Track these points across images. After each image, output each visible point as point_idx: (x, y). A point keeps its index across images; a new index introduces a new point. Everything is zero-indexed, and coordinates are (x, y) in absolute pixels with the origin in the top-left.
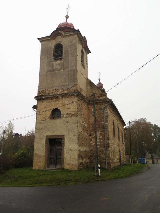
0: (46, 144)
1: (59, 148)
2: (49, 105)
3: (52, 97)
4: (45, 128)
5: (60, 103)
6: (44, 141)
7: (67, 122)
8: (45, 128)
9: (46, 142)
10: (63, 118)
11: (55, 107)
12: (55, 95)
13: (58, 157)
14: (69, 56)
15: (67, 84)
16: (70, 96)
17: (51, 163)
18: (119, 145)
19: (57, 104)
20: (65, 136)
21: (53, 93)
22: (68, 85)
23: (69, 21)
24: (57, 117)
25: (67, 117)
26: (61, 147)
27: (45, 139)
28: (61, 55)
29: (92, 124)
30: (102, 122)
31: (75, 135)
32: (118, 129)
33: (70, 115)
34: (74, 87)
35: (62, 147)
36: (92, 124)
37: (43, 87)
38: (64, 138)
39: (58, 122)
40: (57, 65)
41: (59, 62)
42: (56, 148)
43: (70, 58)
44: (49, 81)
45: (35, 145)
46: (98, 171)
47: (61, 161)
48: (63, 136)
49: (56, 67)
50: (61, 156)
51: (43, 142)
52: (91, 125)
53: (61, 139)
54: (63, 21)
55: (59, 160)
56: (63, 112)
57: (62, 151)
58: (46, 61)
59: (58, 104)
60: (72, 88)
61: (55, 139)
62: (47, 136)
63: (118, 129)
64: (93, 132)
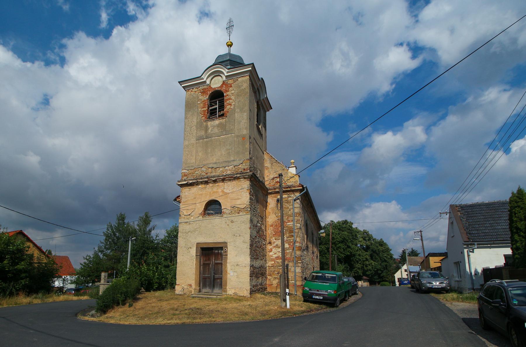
0: (196, 256)
1: (218, 262)
2: (201, 195)
3: (206, 181)
4: (195, 231)
5: (220, 190)
6: (193, 251)
7: (232, 222)
8: (195, 231)
9: (196, 253)
10: (225, 216)
11: (213, 198)
12: (212, 177)
13: (216, 276)
14: (235, 111)
15: (232, 159)
16: (238, 178)
17: (205, 286)
18: (313, 259)
19: (214, 192)
20: (228, 244)
21: (209, 174)
22: (234, 161)
23: (234, 51)
24: (218, 213)
25: (231, 213)
26: (222, 260)
27: (195, 248)
28: (222, 107)
29: (272, 226)
30: (289, 221)
31: (244, 242)
32: (313, 234)
33: (238, 210)
34: (244, 164)
35: (223, 261)
36: (272, 226)
37: (190, 165)
38: (227, 247)
39: (216, 221)
40: (214, 127)
41: (217, 122)
42: (213, 260)
43: (236, 114)
44: (200, 154)
45: (446, 230)
46: (285, 300)
47: (222, 282)
48: (226, 243)
49: (212, 130)
50: (222, 274)
51: (191, 252)
52: (272, 228)
53: (221, 248)
54: (223, 50)
55: (218, 280)
56: (225, 205)
57: (223, 267)
58: (195, 120)
59: (217, 192)
60: (240, 166)
61: (211, 249)
62: (197, 243)
63: (313, 234)
64: (274, 238)
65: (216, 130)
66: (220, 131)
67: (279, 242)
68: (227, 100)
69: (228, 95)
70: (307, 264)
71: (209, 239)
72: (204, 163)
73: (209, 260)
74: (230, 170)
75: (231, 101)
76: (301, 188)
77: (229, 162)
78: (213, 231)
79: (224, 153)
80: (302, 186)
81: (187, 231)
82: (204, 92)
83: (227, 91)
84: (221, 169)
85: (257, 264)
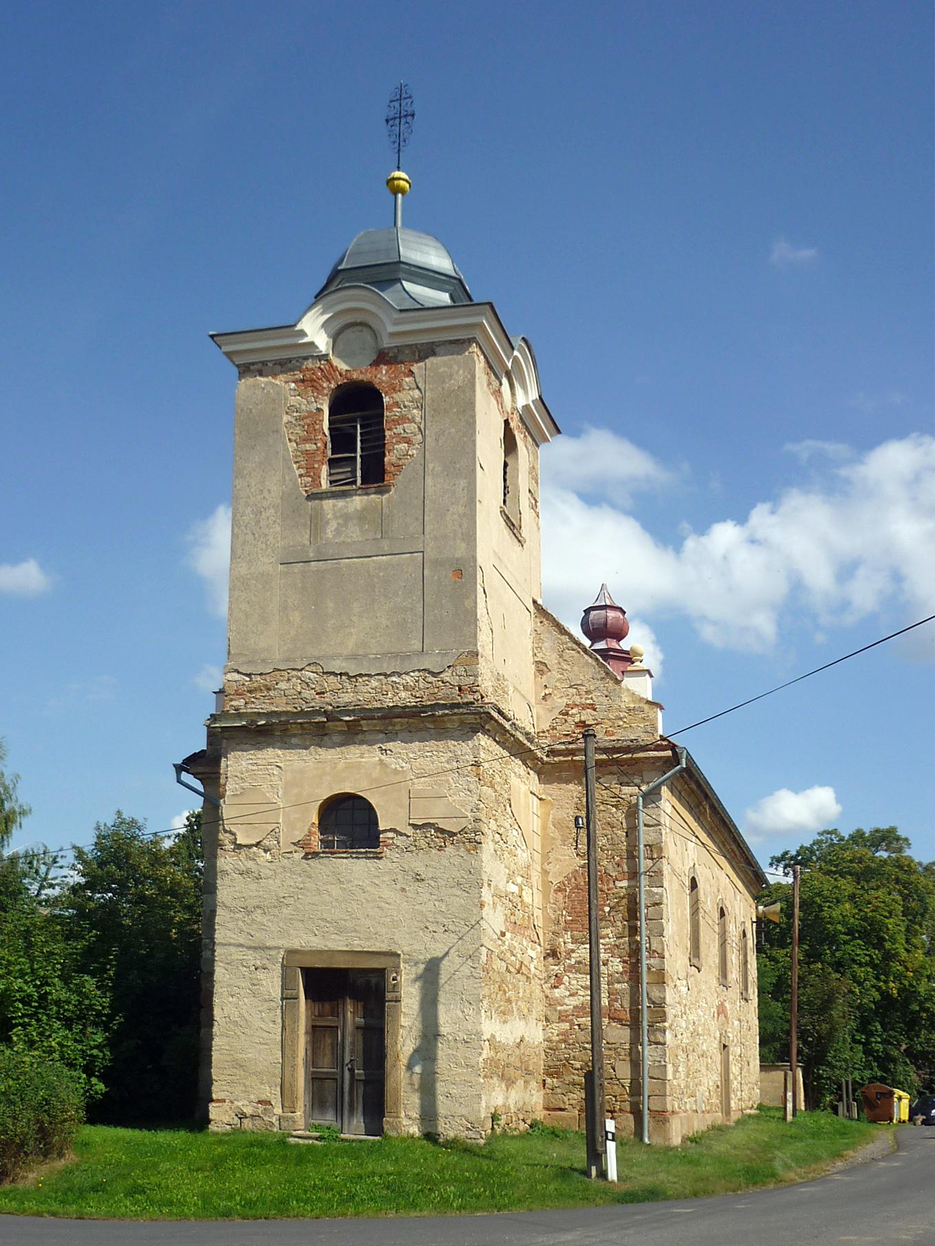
6: (272, 984)
7: (418, 879)
18: (721, 1010)
39: (355, 868)
40: (346, 518)
44: (296, 617)
49: (338, 532)
65: (354, 533)
66: (370, 536)
67: (583, 952)
68: (397, 422)
69: (397, 404)
70: (695, 1034)
71: (336, 937)
72: (313, 652)
73: (334, 1013)
74: (406, 688)
75: (412, 427)
76: (669, 753)
77: (405, 657)
78: (354, 910)
79: (384, 621)
80: (673, 747)
81: (251, 903)
82: (309, 383)
83: (394, 389)
84: (374, 683)
85: (636, 1099)
